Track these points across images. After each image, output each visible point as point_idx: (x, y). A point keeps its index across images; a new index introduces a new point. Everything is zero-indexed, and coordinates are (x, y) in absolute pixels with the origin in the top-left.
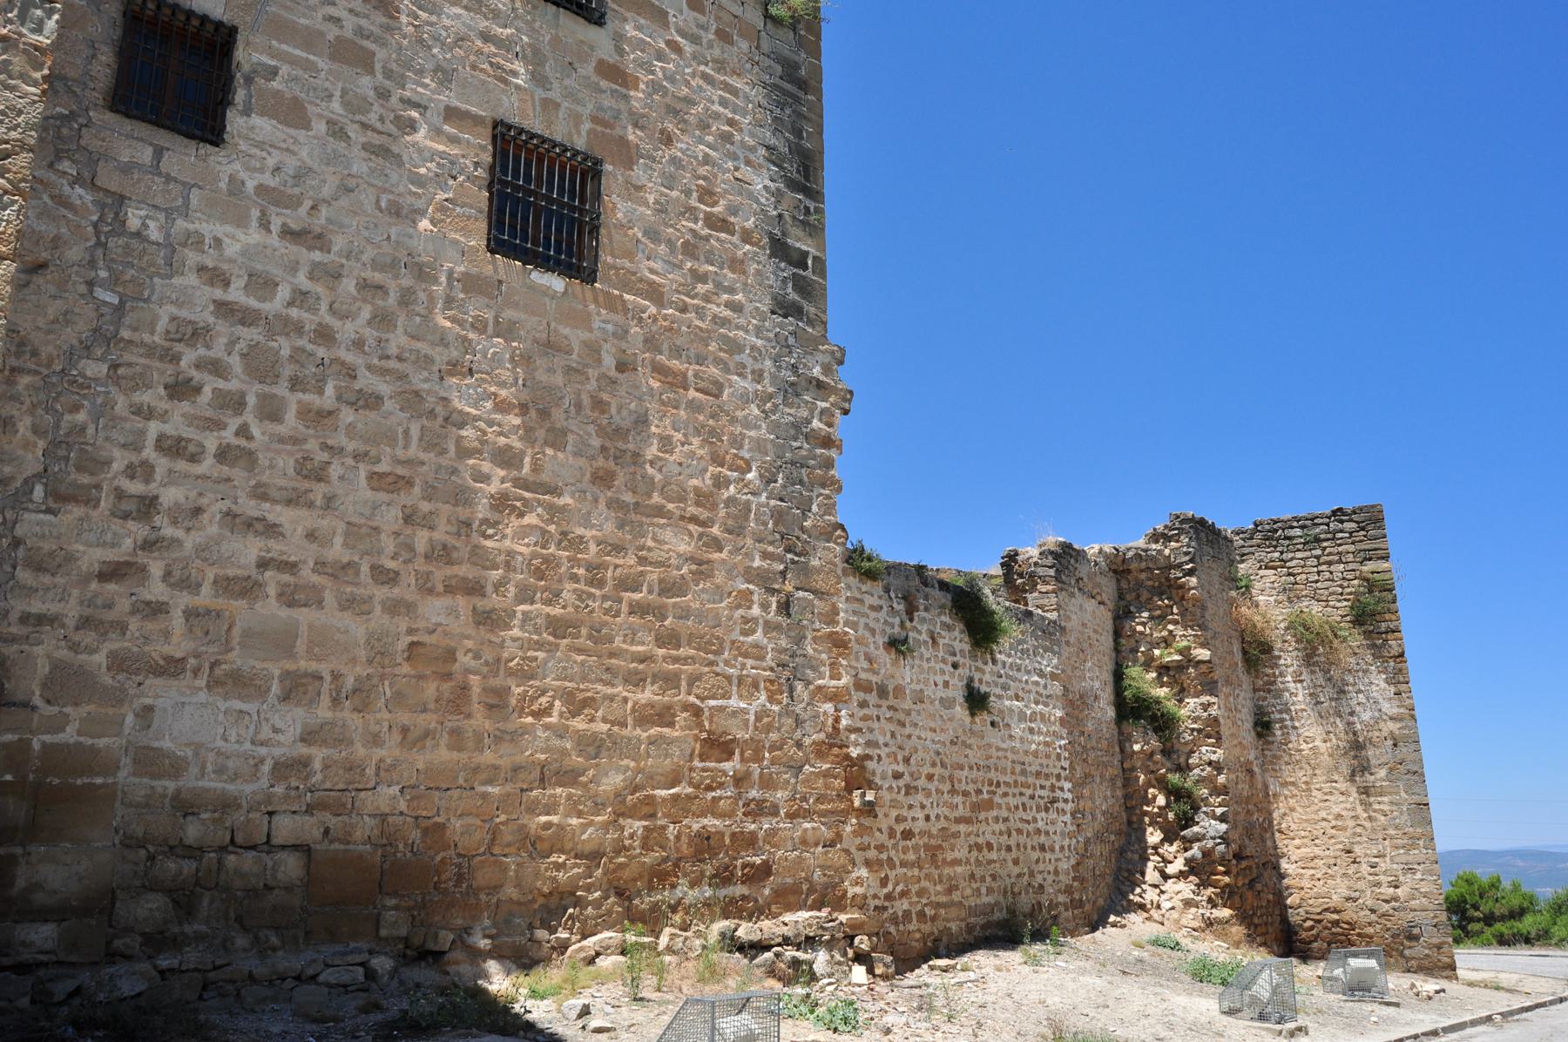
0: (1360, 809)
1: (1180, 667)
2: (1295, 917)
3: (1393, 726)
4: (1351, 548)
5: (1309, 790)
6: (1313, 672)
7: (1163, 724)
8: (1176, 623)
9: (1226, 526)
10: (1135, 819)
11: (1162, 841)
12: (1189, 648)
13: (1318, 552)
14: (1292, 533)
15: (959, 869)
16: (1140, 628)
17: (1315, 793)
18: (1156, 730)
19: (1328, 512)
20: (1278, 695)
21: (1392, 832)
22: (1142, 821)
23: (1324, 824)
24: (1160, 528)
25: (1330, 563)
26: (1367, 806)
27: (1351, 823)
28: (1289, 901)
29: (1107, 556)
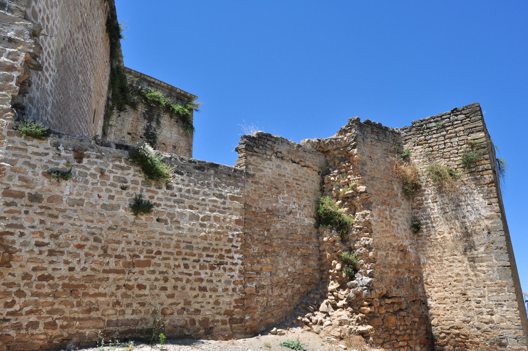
0: (470, 270)
1: (353, 196)
2: (435, 331)
3: (487, 222)
4: (462, 128)
5: (441, 260)
6: (442, 197)
7: (342, 227)
8: (351, 174)
9: (394, 124)
10: (324, 276)
11: (338, 289)
12: (355, 186)
13: (445, 133)
14: (430, 125)
15: (102, 299)
16: (332, 178)
17: (445, 262)
18: (338, 230)
19: (449, 112)
20: (425, 210)
21: (489, 283)
22: (328, 277)
23: (450, 279)
24: (343, 127)
25: (451, 138)
26: (474, 268)
27: (465, 278)
28: (432, 322)
29: (313, 144)
